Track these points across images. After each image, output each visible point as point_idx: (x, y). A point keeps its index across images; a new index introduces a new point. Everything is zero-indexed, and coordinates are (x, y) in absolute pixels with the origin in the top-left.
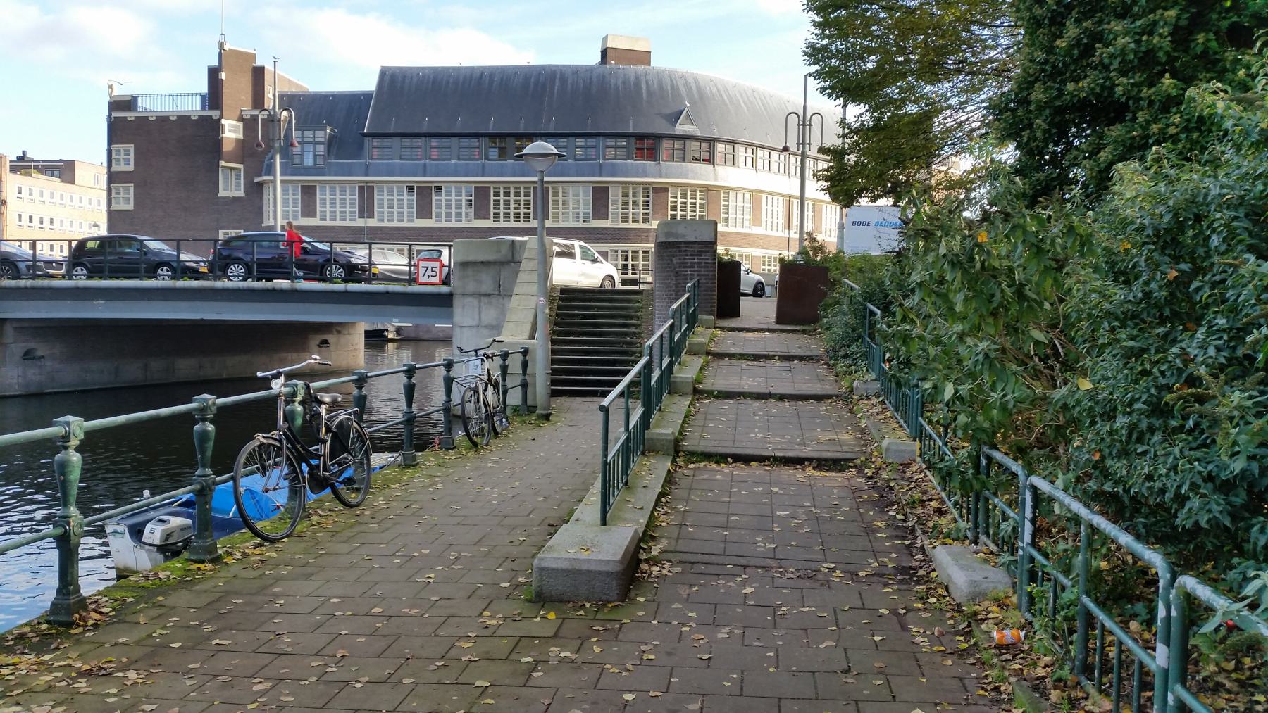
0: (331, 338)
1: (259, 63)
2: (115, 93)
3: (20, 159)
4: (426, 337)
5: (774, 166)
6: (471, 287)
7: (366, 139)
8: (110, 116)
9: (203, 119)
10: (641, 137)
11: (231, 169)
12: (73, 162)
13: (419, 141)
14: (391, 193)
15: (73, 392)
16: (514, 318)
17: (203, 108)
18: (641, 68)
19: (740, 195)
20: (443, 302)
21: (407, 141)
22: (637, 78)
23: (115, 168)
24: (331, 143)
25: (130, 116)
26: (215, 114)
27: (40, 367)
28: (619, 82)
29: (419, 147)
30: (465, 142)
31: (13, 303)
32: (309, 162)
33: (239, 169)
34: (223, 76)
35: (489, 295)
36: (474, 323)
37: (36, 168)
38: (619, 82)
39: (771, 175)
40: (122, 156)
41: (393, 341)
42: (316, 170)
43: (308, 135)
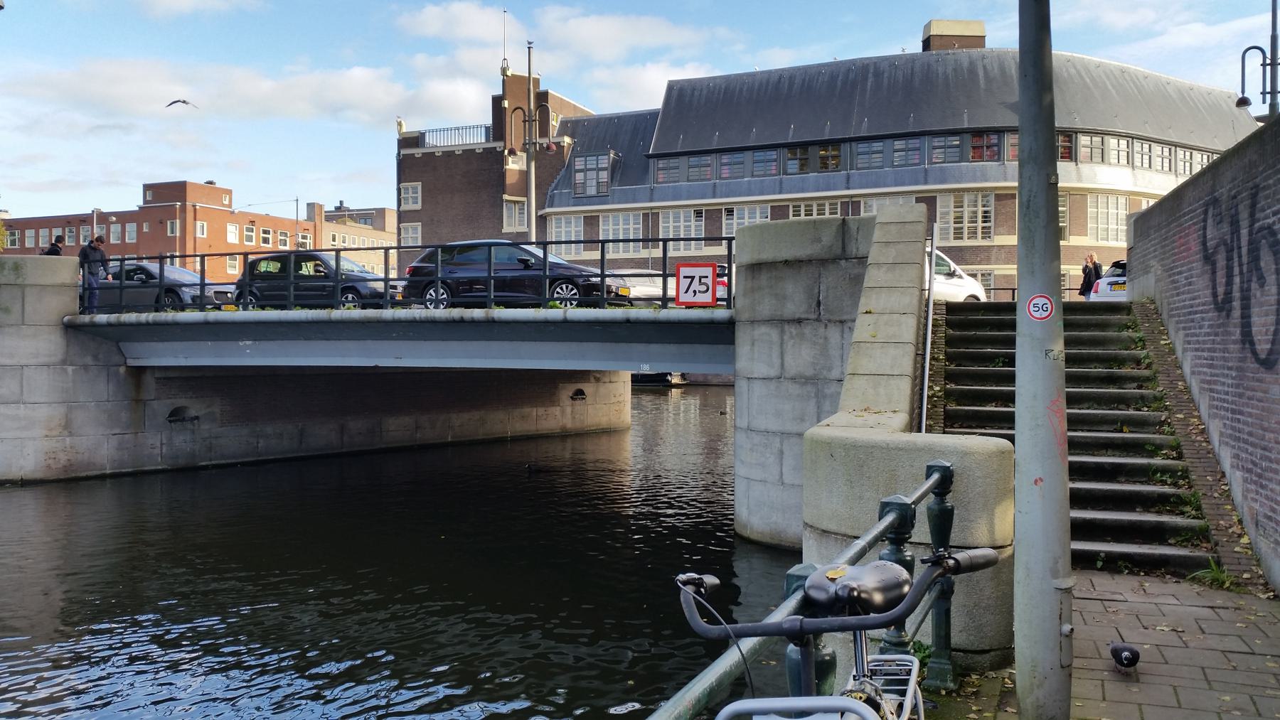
0: (588, 388)
1: (542, 88)
2: (404, 130)
3: (338, 209)
4: (715, 381)
5: (1157, 162)
6: (766, 307)
7: (651, 161)
8: (399, 154)
9: (487, 151)
10: (978, 133)
11: (515, 202)
12: (383, 210)
13: (708, 159)
14: (677, 219)
15: (234, 465)
16: (866, 365)
17: (487, 140)
18: (975, 52)
19: (1112, 199)
20: (720, 334)
21: (693, 160)
22: (972, 63)
23: (404, 207)
24: (614, 168)
25: (417, 152)
26: (498, 145)
27: (193, 432)
28: (949, 70)
29: (709, 166)
30: (760, 155)
31: (160, 345)
32: (592, 191)
33: (522, 203)
34: (506, 104)
35: (799, 321)
36: (773, 372)
37: (351, 217)
38: (949, 70)
39: (1148, 174)
40: (411, 194)
41: (677, 386)
42: (600, 198)
43: (591, 162)
